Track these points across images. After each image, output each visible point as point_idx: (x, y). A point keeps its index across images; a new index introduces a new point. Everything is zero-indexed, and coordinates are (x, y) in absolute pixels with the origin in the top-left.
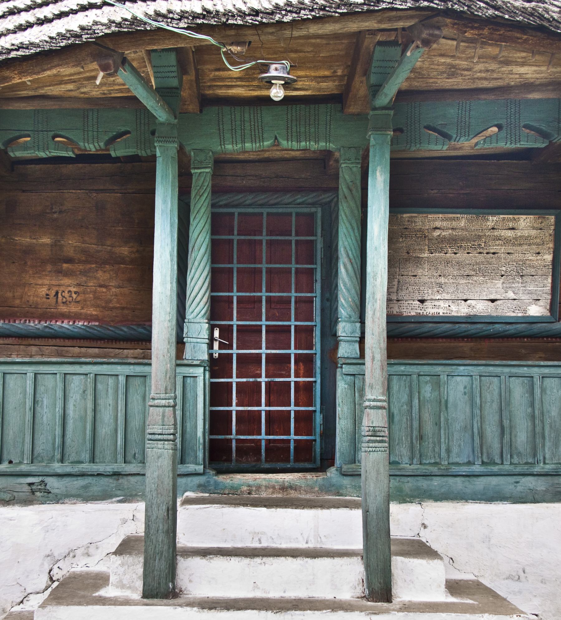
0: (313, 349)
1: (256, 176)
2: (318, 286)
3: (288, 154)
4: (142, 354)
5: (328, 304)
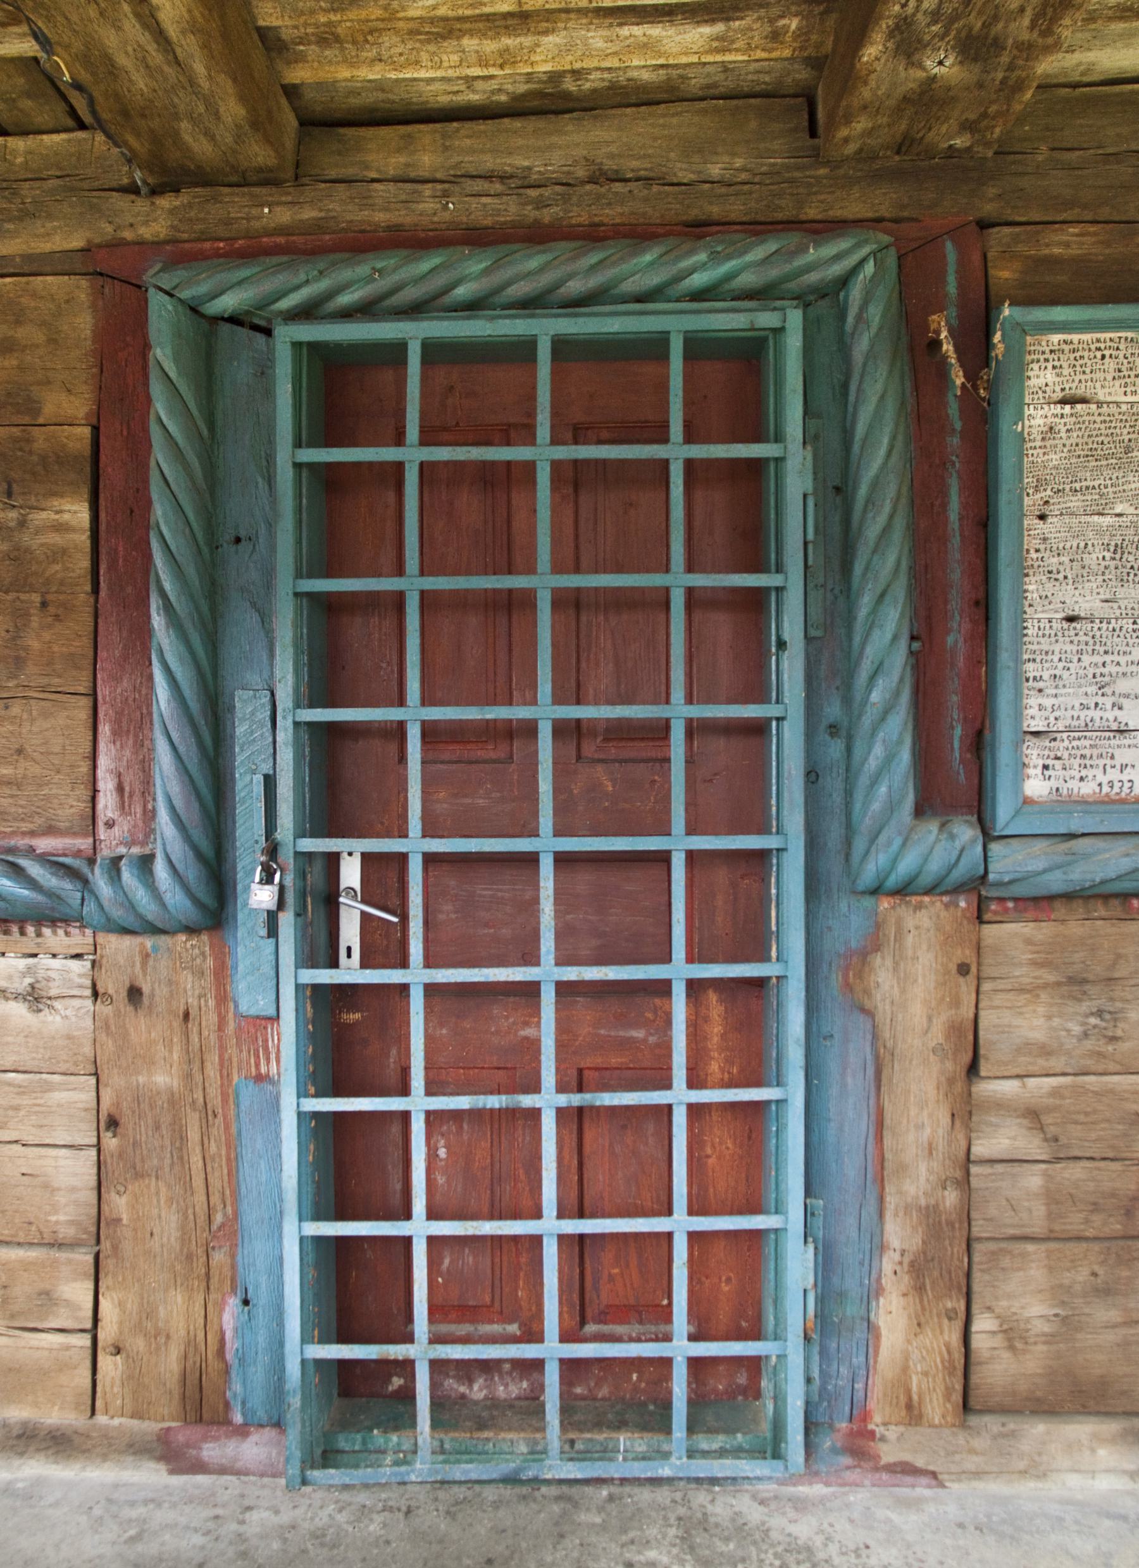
0: (768, 959)
1: (503, 178)
2: (790, 671)
3: (646, 47)
4: (24, 975)
5: (835, 749)
